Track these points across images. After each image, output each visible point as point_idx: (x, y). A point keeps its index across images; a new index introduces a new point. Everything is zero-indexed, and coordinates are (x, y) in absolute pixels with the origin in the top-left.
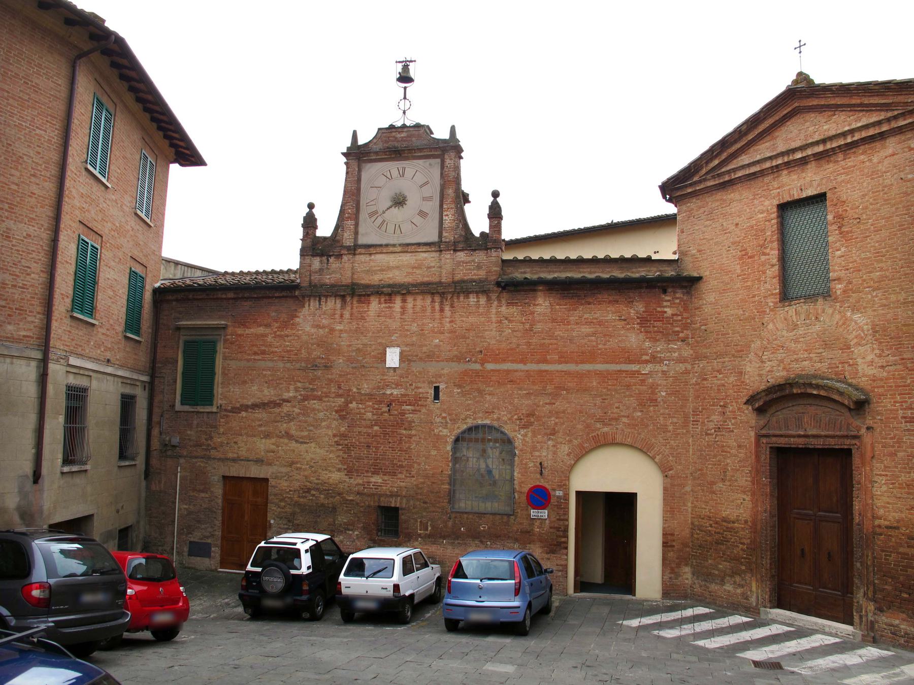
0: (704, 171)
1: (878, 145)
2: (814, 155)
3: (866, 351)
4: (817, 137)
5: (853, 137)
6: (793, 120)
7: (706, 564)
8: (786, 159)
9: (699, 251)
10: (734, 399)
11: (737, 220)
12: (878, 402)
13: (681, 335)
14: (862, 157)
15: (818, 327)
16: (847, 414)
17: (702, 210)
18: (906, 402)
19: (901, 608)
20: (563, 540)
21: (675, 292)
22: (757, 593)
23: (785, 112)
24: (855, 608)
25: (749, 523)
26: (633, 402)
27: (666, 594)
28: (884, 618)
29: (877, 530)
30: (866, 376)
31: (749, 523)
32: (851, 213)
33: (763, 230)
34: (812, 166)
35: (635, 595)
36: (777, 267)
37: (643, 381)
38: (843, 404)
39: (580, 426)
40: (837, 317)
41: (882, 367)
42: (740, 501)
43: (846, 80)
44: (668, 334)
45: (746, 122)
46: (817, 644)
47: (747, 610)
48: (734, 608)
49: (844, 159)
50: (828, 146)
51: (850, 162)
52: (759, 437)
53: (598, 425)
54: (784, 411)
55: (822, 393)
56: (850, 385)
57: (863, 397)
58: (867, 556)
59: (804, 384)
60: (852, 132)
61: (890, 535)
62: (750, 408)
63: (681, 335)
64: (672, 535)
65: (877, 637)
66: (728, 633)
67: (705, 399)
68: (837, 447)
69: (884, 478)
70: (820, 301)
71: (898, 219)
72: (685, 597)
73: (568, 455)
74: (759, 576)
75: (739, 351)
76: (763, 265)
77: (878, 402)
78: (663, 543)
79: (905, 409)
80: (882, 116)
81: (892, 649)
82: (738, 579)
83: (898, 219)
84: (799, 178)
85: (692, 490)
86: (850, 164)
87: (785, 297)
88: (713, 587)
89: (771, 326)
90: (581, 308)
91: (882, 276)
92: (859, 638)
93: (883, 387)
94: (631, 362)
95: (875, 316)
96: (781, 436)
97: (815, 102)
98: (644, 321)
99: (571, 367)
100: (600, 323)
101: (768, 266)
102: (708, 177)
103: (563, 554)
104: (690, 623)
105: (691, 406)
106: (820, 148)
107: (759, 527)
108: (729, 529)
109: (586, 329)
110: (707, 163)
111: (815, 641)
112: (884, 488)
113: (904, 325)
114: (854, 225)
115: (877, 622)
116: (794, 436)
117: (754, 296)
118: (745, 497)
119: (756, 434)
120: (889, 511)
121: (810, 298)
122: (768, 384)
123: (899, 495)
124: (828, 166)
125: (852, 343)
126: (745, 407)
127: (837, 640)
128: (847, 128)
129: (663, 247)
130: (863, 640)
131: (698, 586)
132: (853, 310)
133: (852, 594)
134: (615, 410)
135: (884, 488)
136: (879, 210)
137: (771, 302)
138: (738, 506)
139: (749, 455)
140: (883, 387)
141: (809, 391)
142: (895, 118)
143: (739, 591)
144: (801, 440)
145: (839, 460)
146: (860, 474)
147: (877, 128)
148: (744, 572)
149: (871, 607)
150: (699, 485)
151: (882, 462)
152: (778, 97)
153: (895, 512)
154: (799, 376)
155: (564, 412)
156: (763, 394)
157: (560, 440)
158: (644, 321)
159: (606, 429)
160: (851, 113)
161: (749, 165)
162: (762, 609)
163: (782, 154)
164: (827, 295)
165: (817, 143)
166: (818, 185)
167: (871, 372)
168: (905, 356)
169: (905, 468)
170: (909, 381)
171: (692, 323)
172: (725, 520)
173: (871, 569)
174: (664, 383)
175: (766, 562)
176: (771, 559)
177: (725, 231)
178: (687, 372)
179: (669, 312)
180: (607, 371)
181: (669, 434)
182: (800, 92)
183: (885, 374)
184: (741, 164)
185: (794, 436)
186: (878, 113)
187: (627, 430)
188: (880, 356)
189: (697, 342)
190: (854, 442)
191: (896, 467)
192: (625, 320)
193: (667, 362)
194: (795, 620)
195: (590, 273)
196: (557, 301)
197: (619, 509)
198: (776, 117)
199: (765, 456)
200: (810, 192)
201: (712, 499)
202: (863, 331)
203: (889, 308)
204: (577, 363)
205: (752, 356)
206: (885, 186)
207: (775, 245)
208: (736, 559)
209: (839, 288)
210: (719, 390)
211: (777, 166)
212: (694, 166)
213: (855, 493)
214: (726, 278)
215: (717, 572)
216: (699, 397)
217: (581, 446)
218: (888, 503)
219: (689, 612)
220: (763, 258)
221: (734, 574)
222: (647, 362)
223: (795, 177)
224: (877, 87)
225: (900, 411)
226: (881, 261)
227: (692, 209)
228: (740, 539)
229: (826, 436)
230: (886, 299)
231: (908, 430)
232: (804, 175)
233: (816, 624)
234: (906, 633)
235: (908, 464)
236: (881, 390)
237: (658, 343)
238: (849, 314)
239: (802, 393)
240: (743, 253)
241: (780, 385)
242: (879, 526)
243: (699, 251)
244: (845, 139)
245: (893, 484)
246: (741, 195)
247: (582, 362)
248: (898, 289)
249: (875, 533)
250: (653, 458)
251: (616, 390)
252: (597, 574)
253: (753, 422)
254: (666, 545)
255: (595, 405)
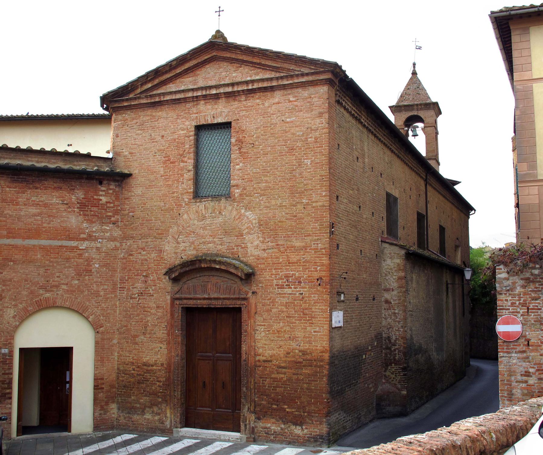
0: (139, 91)
1: (269, 94)
2: (225, 93)
3: (254, 238)
4: (227, 81)
5: (253, 85)
6: (211, 64)
7: (130, 400)
8: (204, 93)
9: (131, 153)
10: (155, 270)
11: (163, 133)
12: (260, 274)
13: (113, 219)
14: (258, 101)
15: (220, 219)
16: (239, 282)
17: (135, 121)
18: (279, 274)
19: (272, 415)
20: (8, 391)
21: (109, 184)
22: (171, 418)
23: (206, 58)
24: (241, 419)
25: (165, 366)
26: (71, 272)
27: (97, 427)
28: (261, 424)
29: (258, 363)
30: (253, 256)
31: (165, 366)
32: (248, 139)
33: (183, 144)
34: (222, 102)
35: (70, 432)
36: (192, 173)
37: (81, 255)
38: (237, 276)
39: (25, 293)
40: (235, 213)
41: (264, 250)
42: (158, 348)
43: (252, 45)
44: (102, 218)
45: (176, 59)
46: (219, 449)
47: (163, 432)
48: (153, 431)
49: (246, 100)
50: (236, 89)
51: (249, 103)
52: (173, 300)
53: (41, 292)
54: (193, 280)
55: (223, 267)
56: (242, 262)
57: (251, 271)
58: (251, 382)
59: (210, 261)
60: (253, 82)
61: (266, 367)
62: (167, 278)
63: (113, 219)
64: (102, 379)
65: (256, 437)
66: (154, 450)
67: (130, 270)
68: (231, 306)
69: (263, 327)
70: (223, 200)
71: (279, 148)
72: (112, 428)
73: (14, 317)
74: (172, 405)
75: (159, 234)
76: (182, 169)
77: (260, 274)
78: (95, 386)
79: (278, 279)
80: (273, 75)
81: (266, 444)
82: (155, 409)
83: (279, 148)
84: (213, 109)
85: (118, 343)
86: (249, 104)
87: (197, 195)
88: (136, 417)
89: (185, 216)
90: (29, 191)
91: (266, 187)
92: (245, 440)
93: (264, 264)
94: (70, 239)
95: (260, 214)
96: (191, 299)
97: (228, 55)
98: (82, 206)
99: (19, 242)
100: (46, 205)
101: (185, 171)
102: (143, 95)
103: (8, 404)
104: (124, 447)
105: (118, 275)
106: (230, 89)
107: (172, 368)
108: (148, 371)
109: (33, 210)
110: (142, 85)
111: (217, 447)
112: (263, 334)
113: (279, 222)
114: (250, 148)
115: (256, 427)
116: (200, 299)
117: (173, 193)
118: (162, 345)
119: (171, 297)
120: (265, 350)
121: (216, 197)
122: (182, 260)
123: (272, 338)
124: (233, 103)
125: (244, 232)
126: (163, 277)
127: (231, 444)
128: (249, 79)
129: (97, 144)
130: (247, 441)
131: (122, 418)
132: (246, 209)
133: (240, 410)
134: (56, 279)
135: (263, 334)
136: (267, 140)
137: (186, 198)
138: (157, 353)
139: (165, 313)
140: (264, 264)
141: (213, 265)
142: (282, 78)
143: (157, 418)
144: (205, 302)
145: (232, 316)
146: (247, 325)
147: (269, 82)
148: (160, 403)
149: (253, 417)
150: (125, 338)
151: (262, 316)
152: (202, 46)
153: (269, 350)
154: (206, 255)
155: (10, 280)
156: (179, 267)
157: (6, 305)
158: (82, 206)
159: (48, 295)
160: (252, 68)
161: (176, 92)
162: (175, 429)
163: (202, 88)
164: (228, 196)
165: (228, 85)
166: (226, 116)
167: (256, 253)
168: (279, 243)
169: (277, 320)
170: (281, 260)
171: (122, 209)
172: (145, 364)
173: (253, 391)
174: (98, 257)
175: (178, 394)
176: (181, 391)
177: (153, 140)
178: (116, 249)
179: (104, 199)
180: (50, 246)
181: (100, 298)
182: (218, 45)
183: (266, 255)
184: (169, 90)
185: (200, 299)
186: (270, 72)
187: (66, 296)
188: (263, 242)
189: (125, 225)
190: (243, 302)
191: (271, 319)
192: (67, 204)
193: (100, 241)
194: (199, 434)
195: (38, 162)
196: (7, 184)
197: (54, 363)
198: (199, 60)
199: (178, 314)
200: (220, 120)
201: (135, 349)
202: (252, 224)
203: (270, 209)
204: (24, 238)
205: (170, 238)
206: (272, 124)
207: (192, 155)
208: (155, 394)
209: (237, 192)
210: (142, 263)
211: (197, 97)
212: (132, 86)
213: (243, 338)
214: (152, 177)
215: (138, 406)
216: (126, 268)
217: (25, 309)
218: (265, 344)
219: (119, 439)
220: (182, 164)
221: (152, 405)
222: (84, 239)
223: (209, 107)
224: (271, 54)
225: (275, 281)
226: (267, 176)
227: (127, 119)
228: (158, 378)
229: (224, 299)
230: (269, 202)
231: (279, 294)
232: (216, 106)
233: (215, 435)
234: (275, 432)
235: (278, 317)
236: (262, 266)
237: (94, 225)
238: (243, 211)
239: (207, 267)
240: (167, 159)
241: (192, 261)
242: (259, 361)
243: (131, 153)
244: (247, 86)
245: (268, 331)
246: (167, 114)
247: (29, 238)
248: (276, 196)
249: (256, 366)
250: (87, 318)
251: (57, 262)
252: (34, 420)
253: (169, 289)
254: (97, 388)
255: (39, 274)
